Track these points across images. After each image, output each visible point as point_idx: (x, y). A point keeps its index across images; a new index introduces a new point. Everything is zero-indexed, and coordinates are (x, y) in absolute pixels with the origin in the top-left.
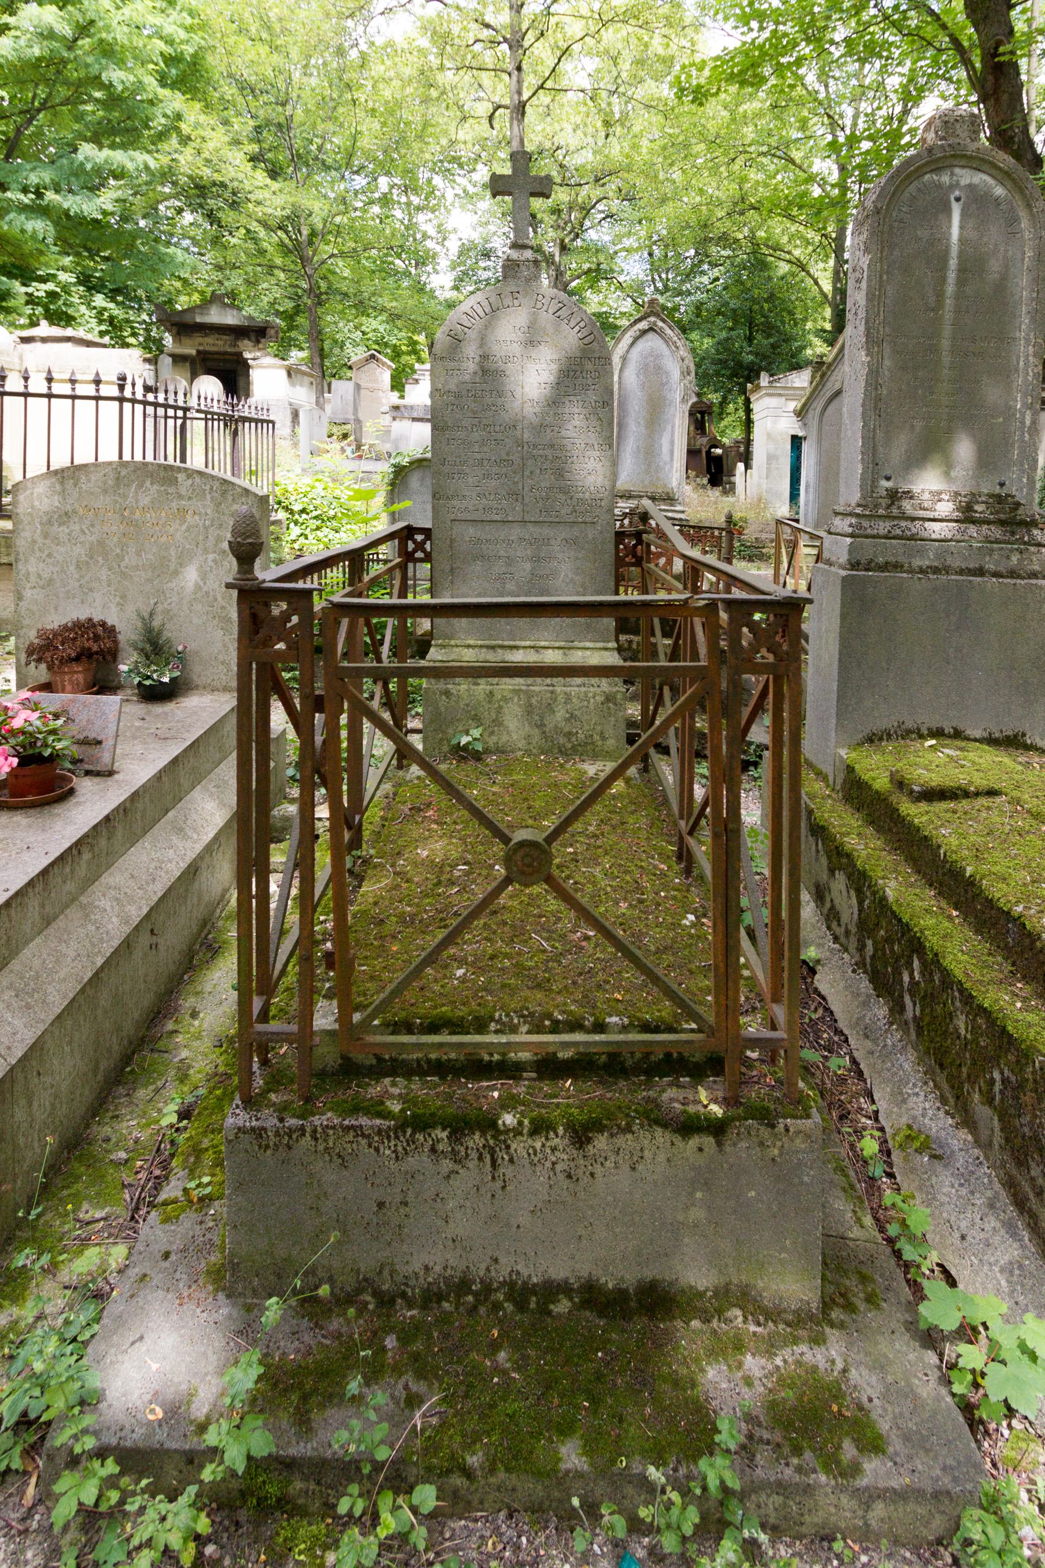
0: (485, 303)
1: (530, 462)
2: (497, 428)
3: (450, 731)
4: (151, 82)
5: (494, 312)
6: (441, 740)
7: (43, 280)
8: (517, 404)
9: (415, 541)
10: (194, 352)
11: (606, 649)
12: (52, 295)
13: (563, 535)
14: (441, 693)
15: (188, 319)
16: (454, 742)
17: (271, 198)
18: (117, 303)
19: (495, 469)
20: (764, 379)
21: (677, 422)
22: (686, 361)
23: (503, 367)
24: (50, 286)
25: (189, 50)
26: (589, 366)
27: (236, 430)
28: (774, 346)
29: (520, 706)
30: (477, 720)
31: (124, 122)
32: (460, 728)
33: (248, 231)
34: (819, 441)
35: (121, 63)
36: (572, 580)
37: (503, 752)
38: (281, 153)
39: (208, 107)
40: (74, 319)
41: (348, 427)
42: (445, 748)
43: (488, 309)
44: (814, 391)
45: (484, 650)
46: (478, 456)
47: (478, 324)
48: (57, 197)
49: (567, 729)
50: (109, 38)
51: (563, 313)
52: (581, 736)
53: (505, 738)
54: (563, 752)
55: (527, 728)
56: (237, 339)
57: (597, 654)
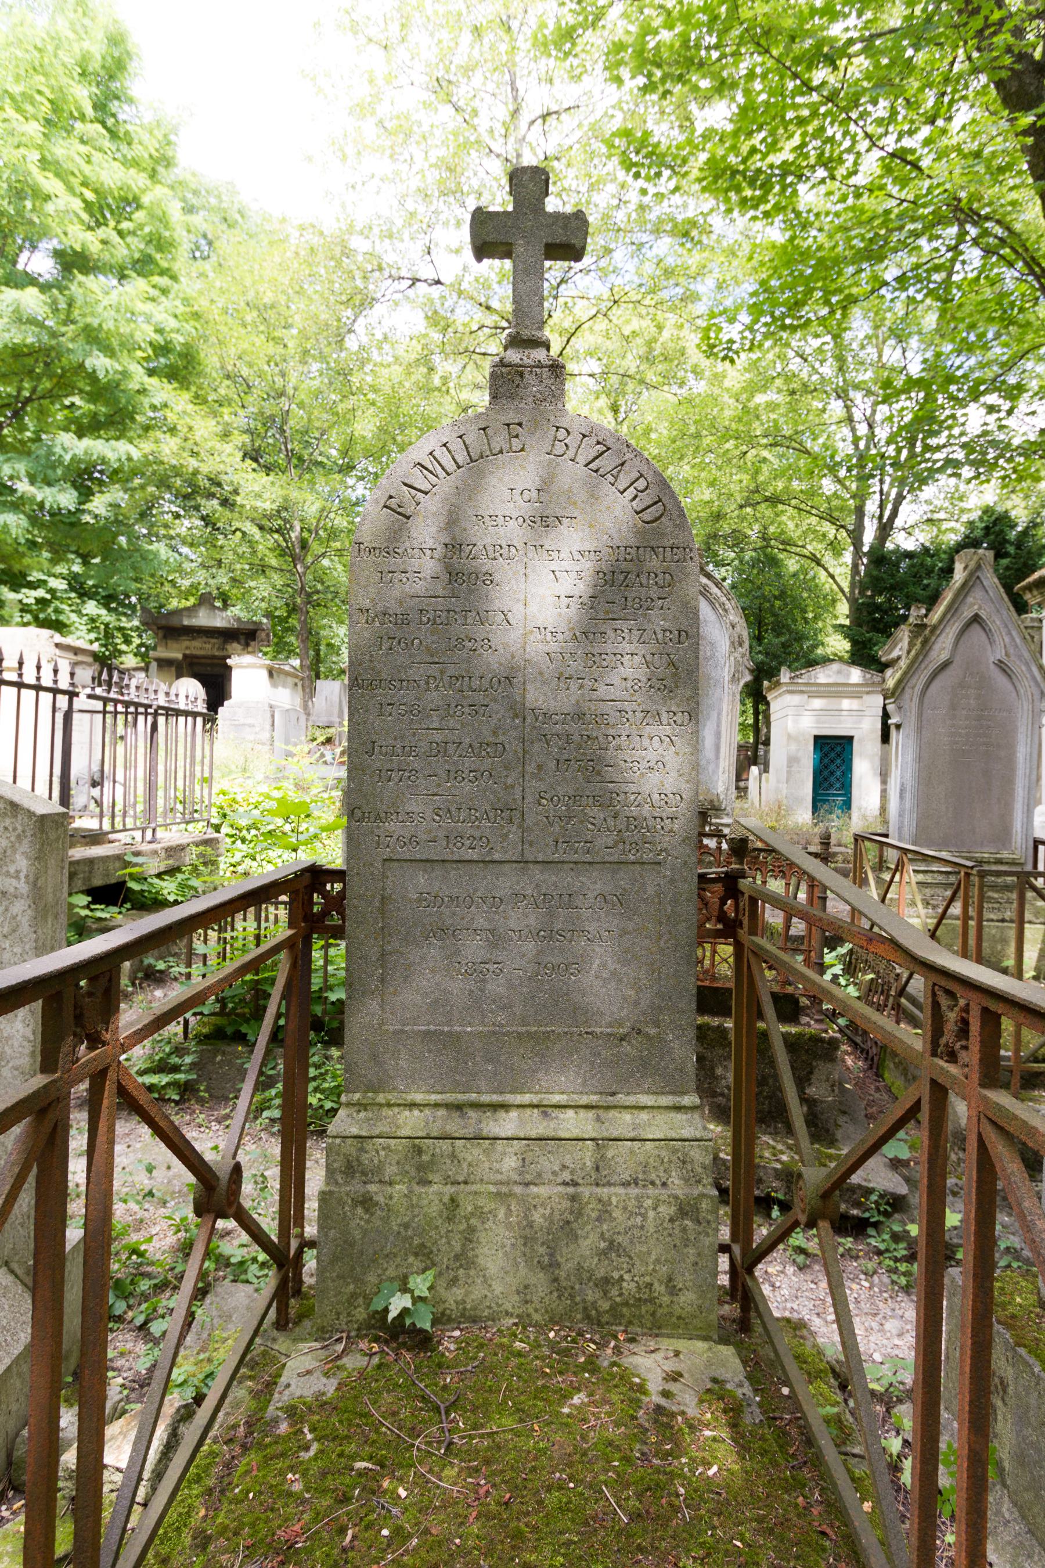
0: (457, 446)
1: (537, 747)
2: (476, 683)
3: (372, 1278)
4: (138, 376)
5: (476, 463)
6: (354, 1296)
7: (33, 586)
8: (514, 636)
9: (325, 895)
10: (180, 656)
11: (678, 1108)
12: (41, 602)
13: (598, 887)
14: (356, 1203)
15: (174, 622)
16: (378, 1305)
17: (259, 491)
18: (109, 610)
19: (469, 763)
20: (785, 676)
21: (725, 708)
22: (738, 628)
23: (486, 565)
24: (41, 593)
25: (179, 339)
26: (653, 563)
27: (154, 727)
28: (784, 645)
29: (509, 1226)
30: (426, 1255)
31: (114, 413)
32: (391, 1272)
33: (244, 533)
34: (920, 729)
35: (109, 351)
36: (614, 973)
37: (474, 1321)
38: (274, 446)
39: (199, 399)
40: (65, 626)
41: (332, 730)
42: (361, 1314)
43: (462, 457)
44: (913, 662)
45: (441, 1112)
46: (438, 737)
47: (445, 486)
48: (32, 490)
49: (601, 1273)
50: (95, 322)
51: (606, 463)
52: (629, 1286)
53: (478, 1291)
54: (593, 1319)
55: (523, 1270)
56: (225, 642)
57: (661, 1118)
